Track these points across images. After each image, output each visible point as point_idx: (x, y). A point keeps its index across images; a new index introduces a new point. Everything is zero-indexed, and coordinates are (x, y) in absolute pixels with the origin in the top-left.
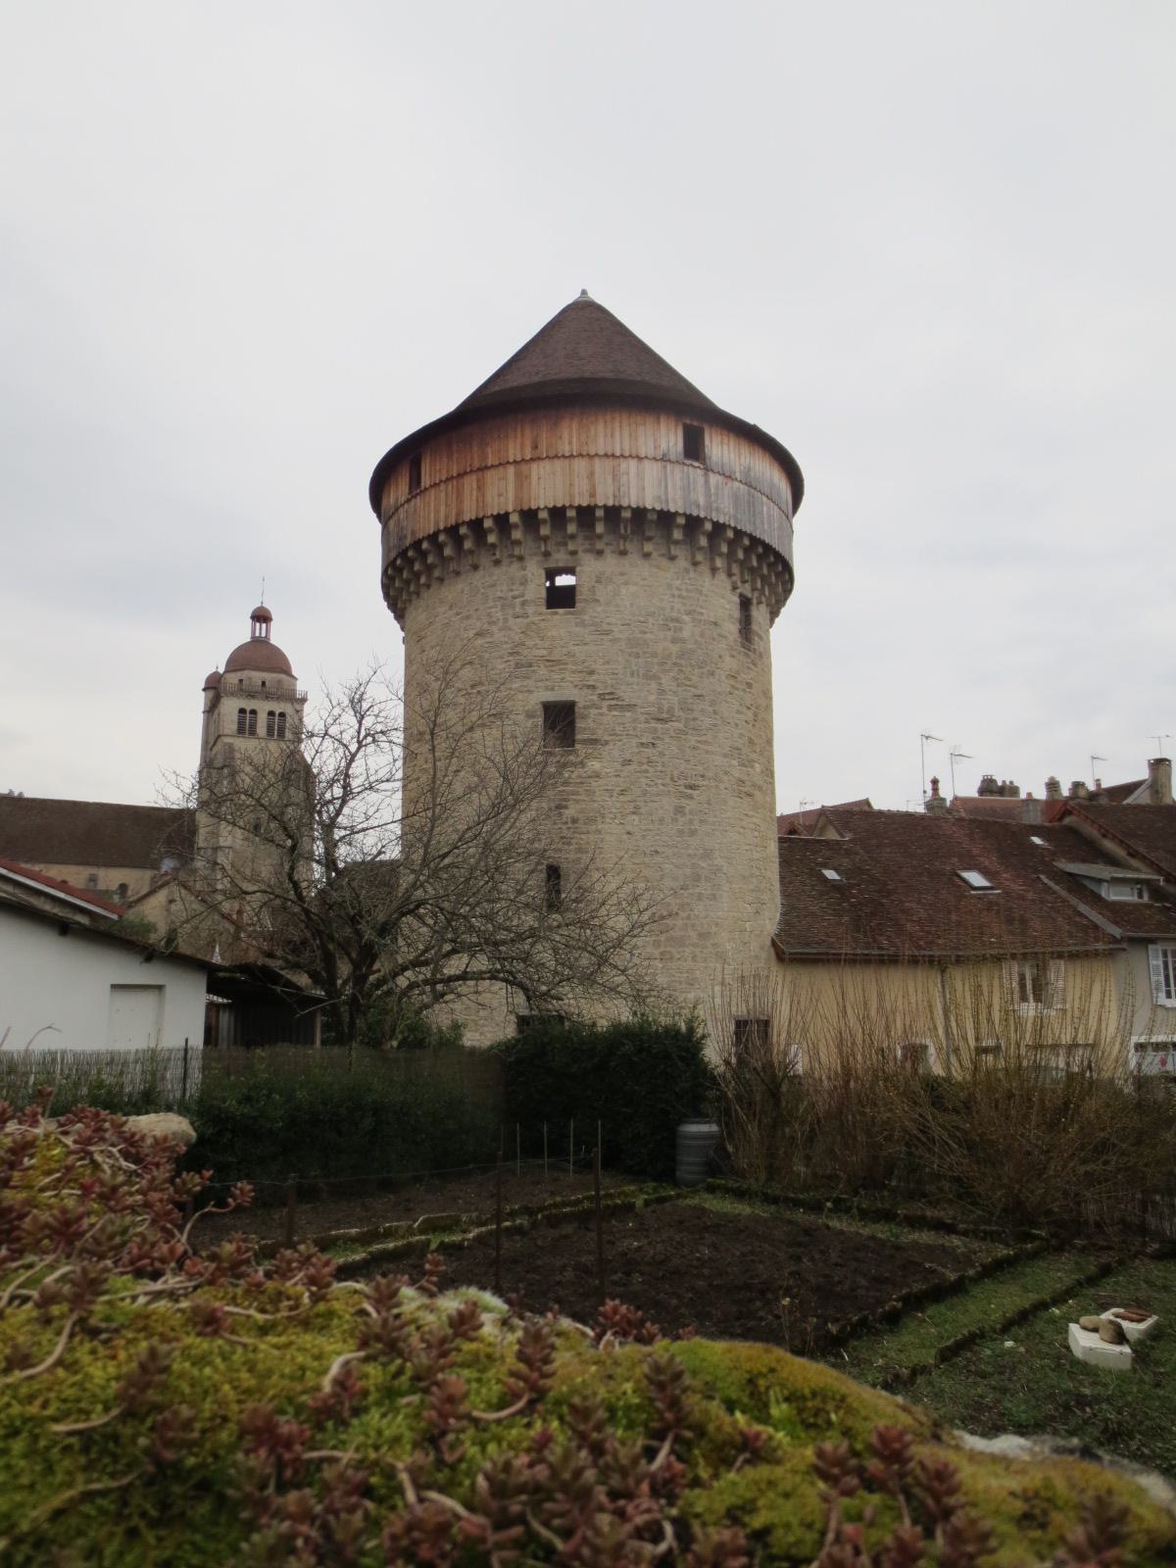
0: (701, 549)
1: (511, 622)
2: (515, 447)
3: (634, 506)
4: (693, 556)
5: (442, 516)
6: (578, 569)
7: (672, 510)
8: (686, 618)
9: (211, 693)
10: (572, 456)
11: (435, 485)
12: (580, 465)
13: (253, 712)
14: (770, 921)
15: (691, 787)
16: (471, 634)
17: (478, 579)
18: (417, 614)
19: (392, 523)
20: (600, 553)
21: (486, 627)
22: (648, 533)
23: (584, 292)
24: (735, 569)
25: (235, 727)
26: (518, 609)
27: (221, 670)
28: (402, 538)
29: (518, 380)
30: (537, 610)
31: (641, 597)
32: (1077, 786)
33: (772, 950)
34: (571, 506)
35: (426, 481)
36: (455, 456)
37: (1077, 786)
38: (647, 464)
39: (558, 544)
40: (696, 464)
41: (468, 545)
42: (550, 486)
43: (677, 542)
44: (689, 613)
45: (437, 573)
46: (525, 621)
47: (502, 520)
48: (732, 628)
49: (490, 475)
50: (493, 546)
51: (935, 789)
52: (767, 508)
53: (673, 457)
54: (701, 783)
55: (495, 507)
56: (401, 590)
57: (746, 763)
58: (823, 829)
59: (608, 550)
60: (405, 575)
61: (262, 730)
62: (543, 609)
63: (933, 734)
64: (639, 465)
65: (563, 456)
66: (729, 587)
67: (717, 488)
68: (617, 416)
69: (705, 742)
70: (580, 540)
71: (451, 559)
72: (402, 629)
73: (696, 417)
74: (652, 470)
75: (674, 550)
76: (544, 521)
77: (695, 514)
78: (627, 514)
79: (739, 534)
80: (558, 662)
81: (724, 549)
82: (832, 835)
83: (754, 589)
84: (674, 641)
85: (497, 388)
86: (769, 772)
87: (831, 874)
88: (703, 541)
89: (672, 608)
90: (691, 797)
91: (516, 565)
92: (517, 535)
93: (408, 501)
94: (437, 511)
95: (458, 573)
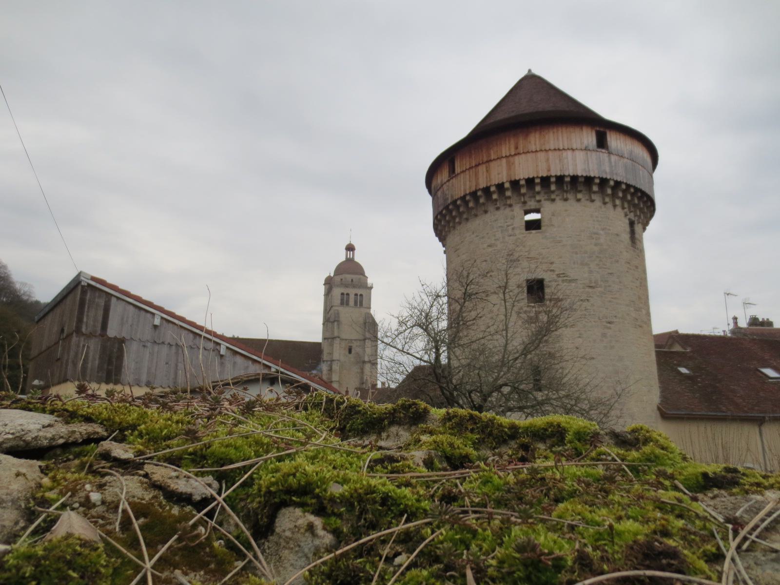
0: (608, 195)
1: (507, 238)
2: (506, 148)
3: (571, 174)
4: (604, 199)
5: (468, 187)
6: (542, 209)
7: (592, 176)
8: (601, 232)
9: (327, 286)
10: (536, 151)
11: (463, 172)
12: (541, 155)
13: (348, 294)
14: (655, 397)
15: (609, 323)
16: (485, 246)
17: (488, 217)
18: (453, 238)
19: (439, 193)
20: (553, 200)
21: (493, 242)
22: (579, 189)
23: (530, 71)
24: (626, 205)
25: (339, 302)
26: (510, 232)
27: (332, 275)
28: (445, 200)
29: (500, 116)
30: (521, 232)
31: (575, 221)
32: (763, 319)
33: (658, 412)
34: (537, 177)
35: (458, 170)
36: (473, 156)
37: (763, 319)
38: (577, 153)
39: (530, 197)
40: (603, 151)
41: (482, 200)
42: (526, 167)
43: (595, 192)
44: (603, 229)
45: (465, 216)
46: (515, 238)
47: (500, 187)
48: (626, 237)
49: (492, 164)
50: (496, 200)
51: (736, 323)
52: (643, 173)
53: (591, 148)
54: (615, 320)
55: (496, 180)
56: (445, 226)
57: (638, 310)
58: (671, 346)
59: (558, 199)
60: (447, 218)
61: (352, 302)
62: (524, 231)
63: (731, 292)
64: (574, 153)
65: (532, 152)
66: (623, 214)
67: (615, 162)
68: (560, 129)
69: (615, 298)
70: (542, 194)
71: (472, 208)
72: (444, 246)
73: (603, 129)
74: (580, 156)
75: (594, 197)
76: (523, 186)
77: (604, 177)
78: (568, 179)
79: (628, 186)
80: (534, 258)
81: (620, 194)
82: (677, 348)
83: (635, 216)
84: (596, 245)
85: (492, 121)
86: (648, 314)
87: (683, 370)
88: (609, 191)
89: (594, 228)
90: (610, 328)
91: (508, 209)
92: (508, 193)
93: (448, 181)
94: (465, 184)
95: (476, 216)
